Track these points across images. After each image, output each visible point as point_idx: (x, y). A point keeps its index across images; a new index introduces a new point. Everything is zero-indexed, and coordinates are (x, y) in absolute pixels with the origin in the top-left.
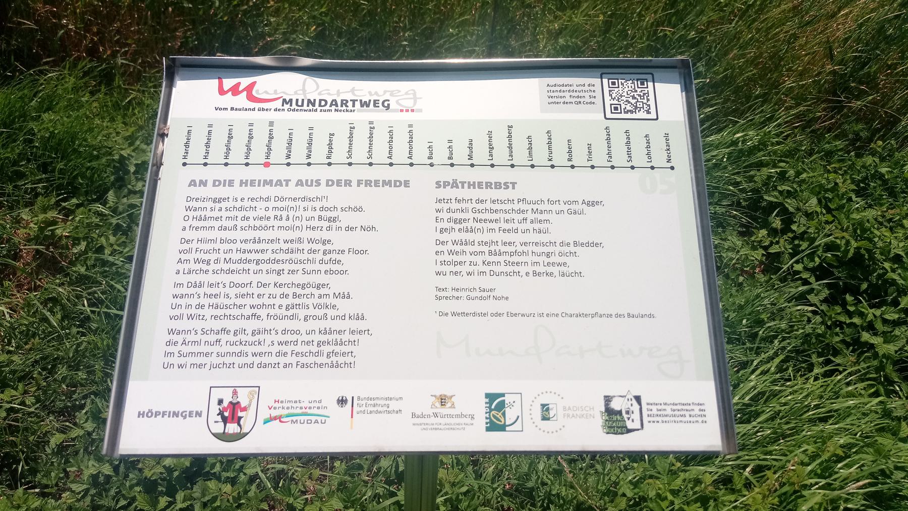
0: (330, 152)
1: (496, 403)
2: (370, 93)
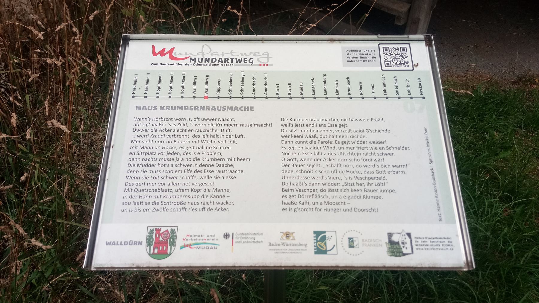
0: (219, 90)
1: (320, 237)
2: (241, 54)
